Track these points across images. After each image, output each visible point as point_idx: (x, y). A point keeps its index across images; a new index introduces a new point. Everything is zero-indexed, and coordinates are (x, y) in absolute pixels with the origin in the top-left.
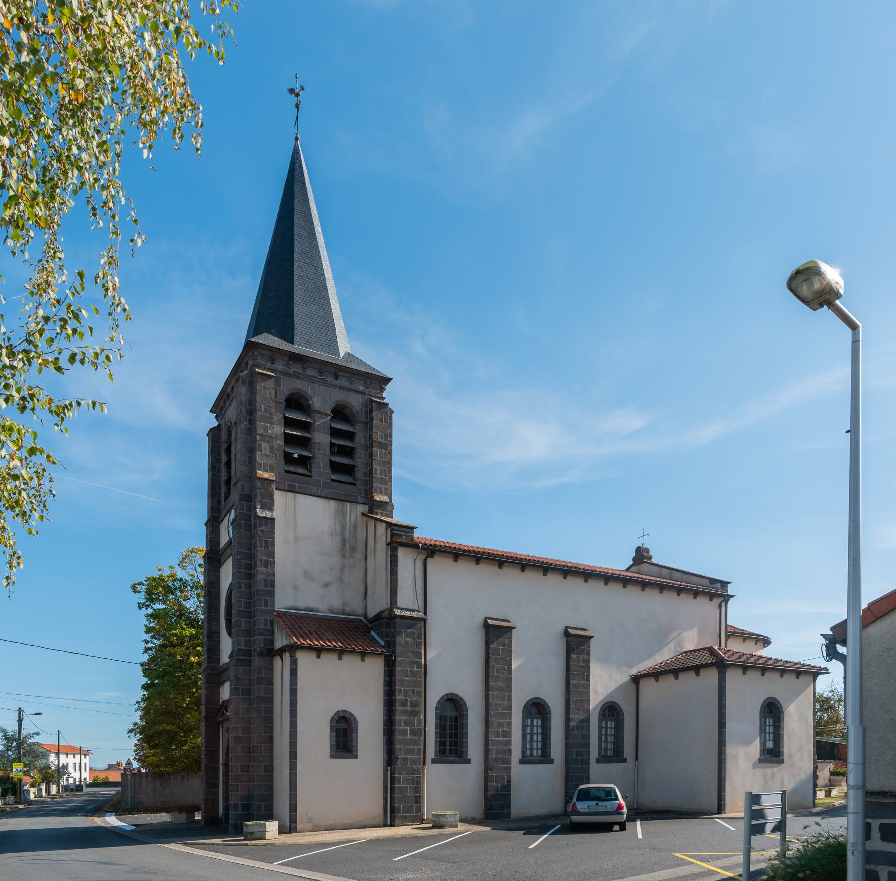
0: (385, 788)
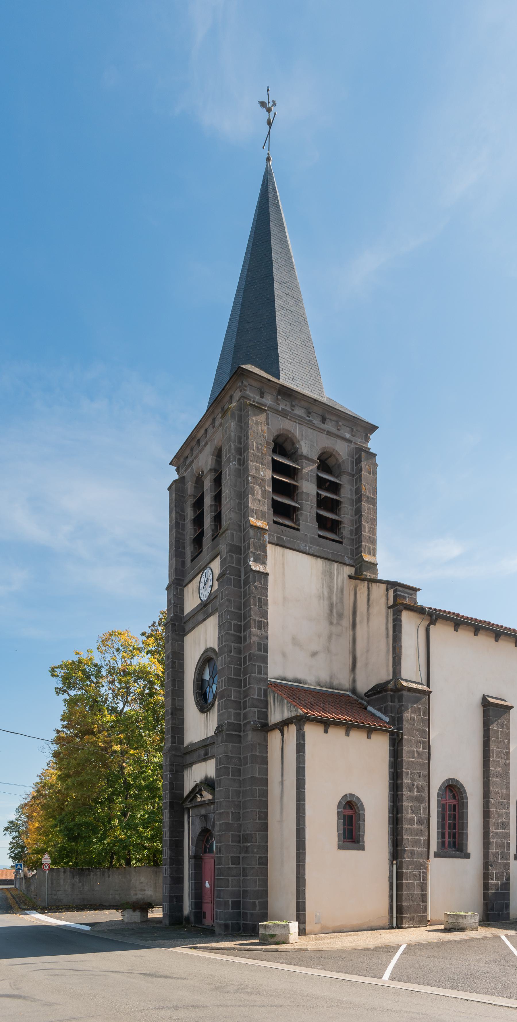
0: (391, 884)
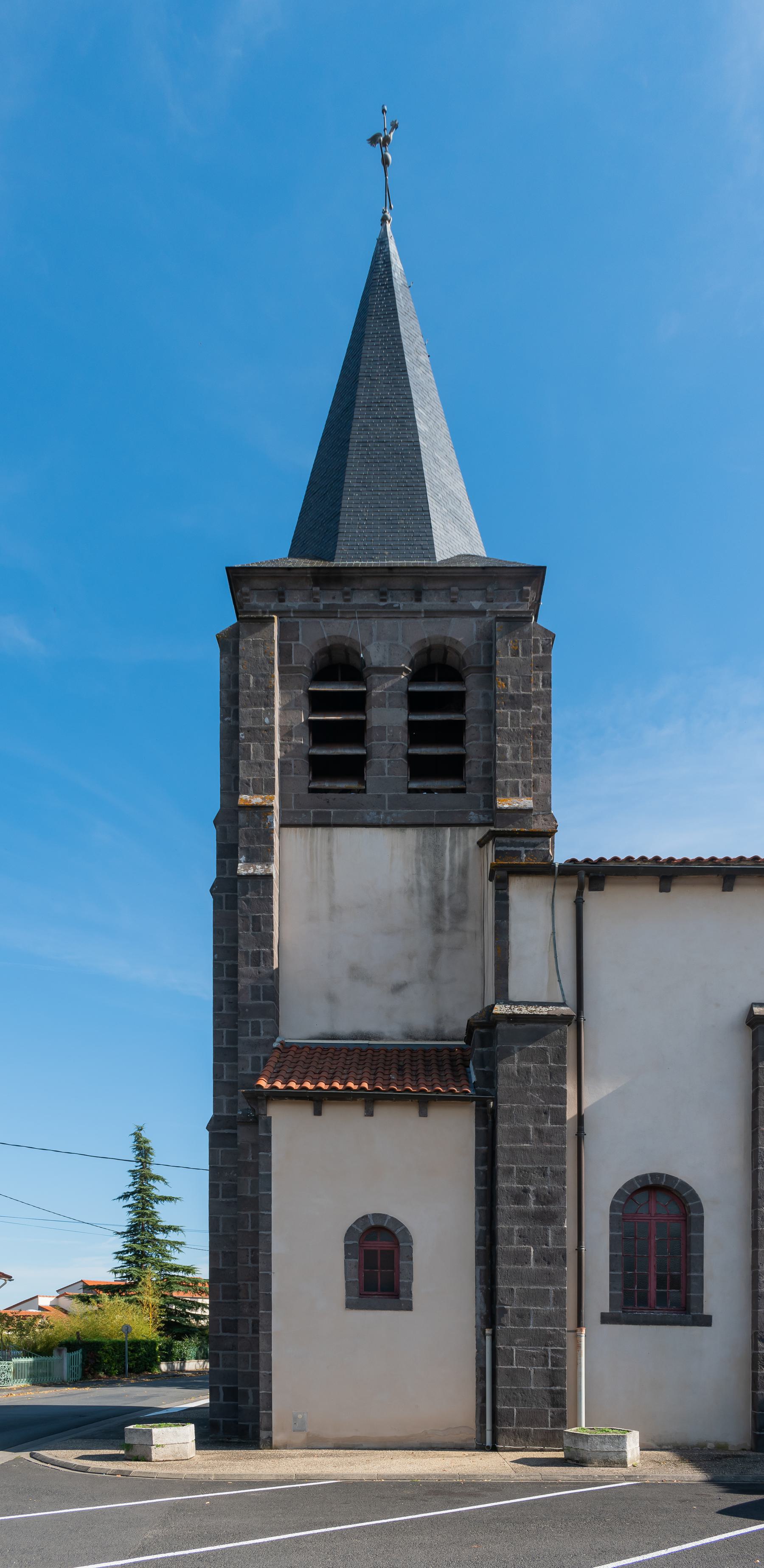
0: (481, 1370)
